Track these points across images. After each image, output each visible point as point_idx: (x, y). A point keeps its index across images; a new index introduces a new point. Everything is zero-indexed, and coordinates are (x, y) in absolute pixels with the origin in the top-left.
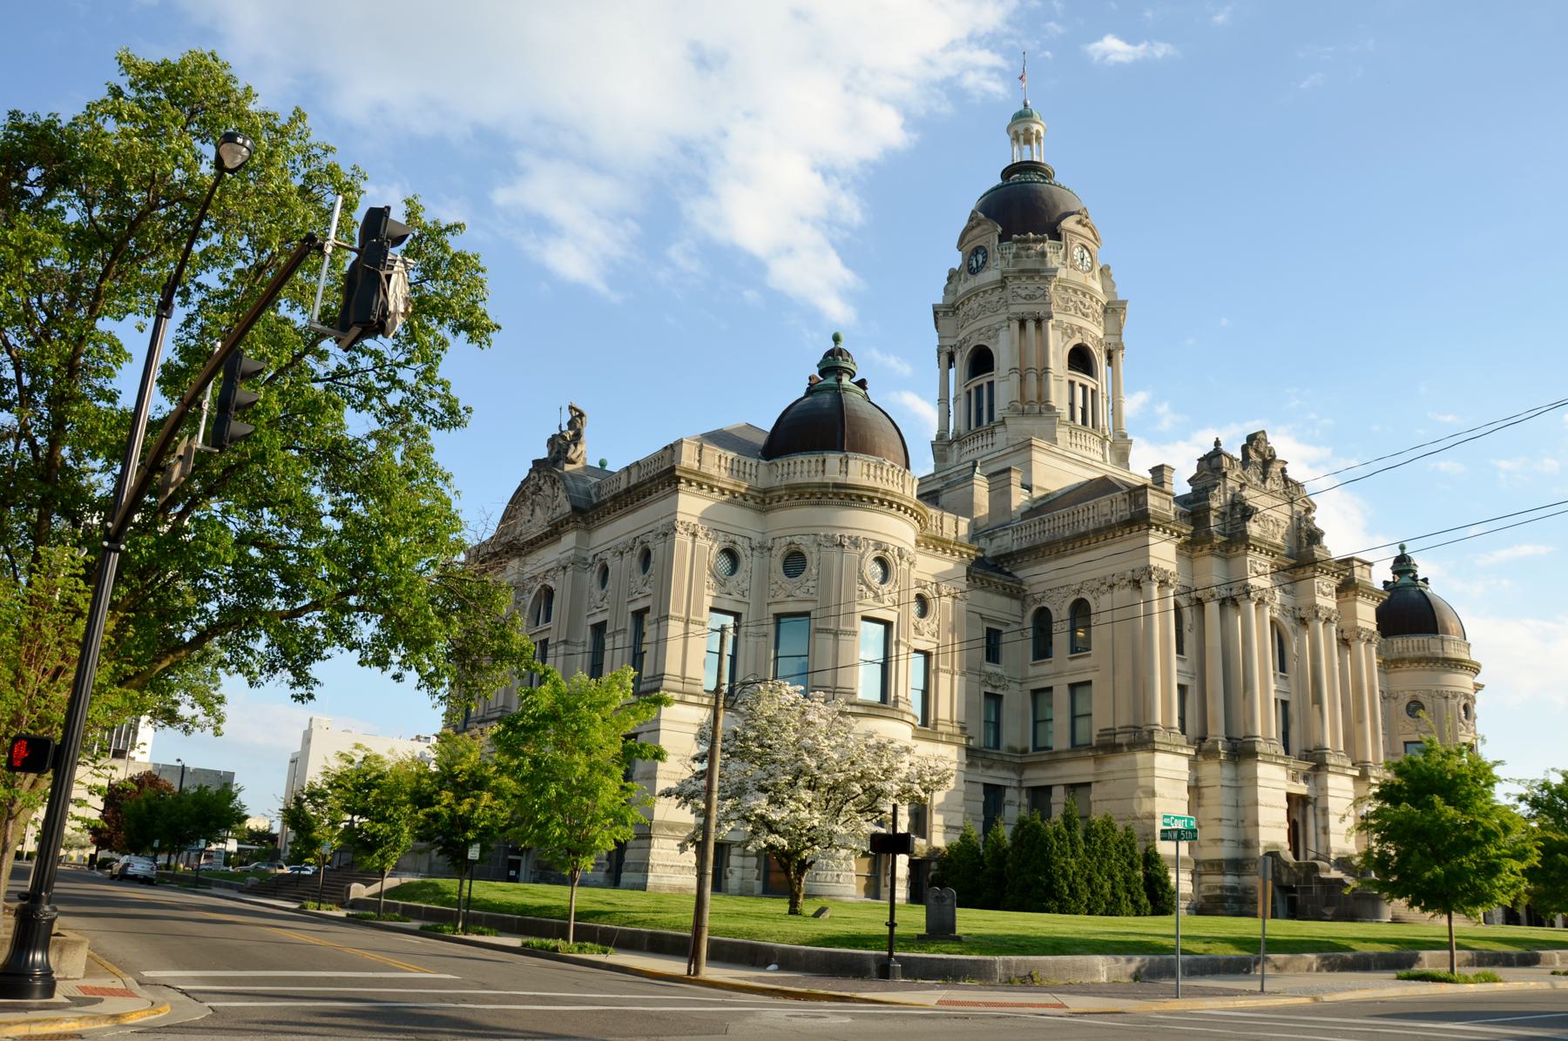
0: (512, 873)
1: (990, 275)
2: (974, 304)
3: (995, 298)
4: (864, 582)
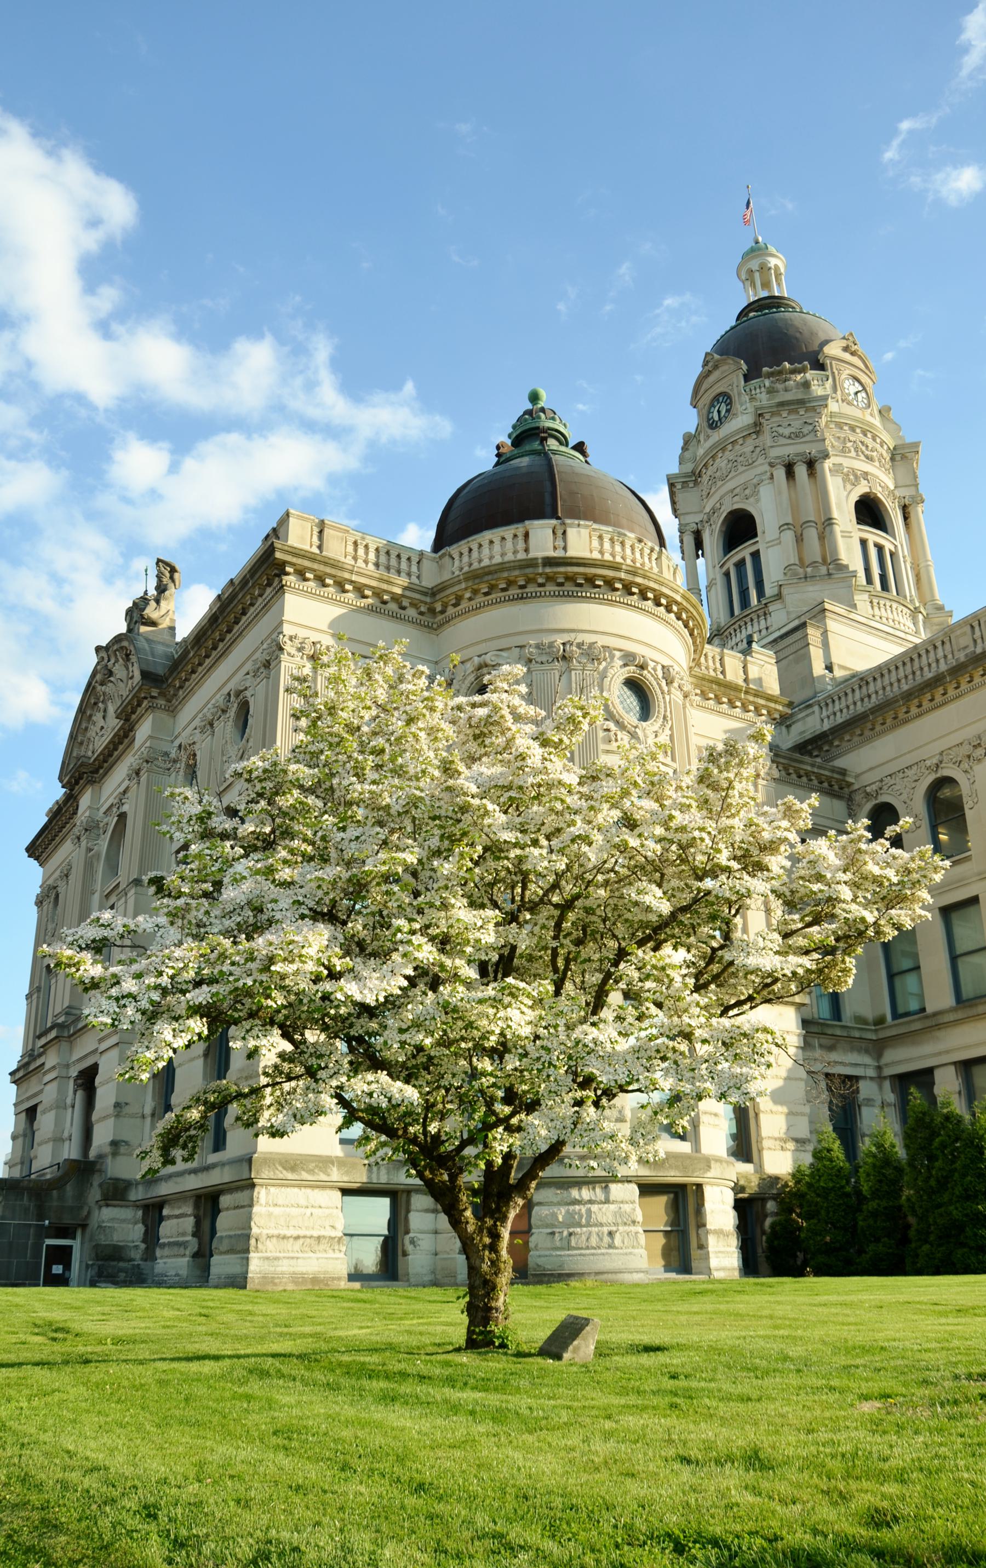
0: (57, 1269)
1: (742, 420)
2: (721, 462)
3: (748, 448)
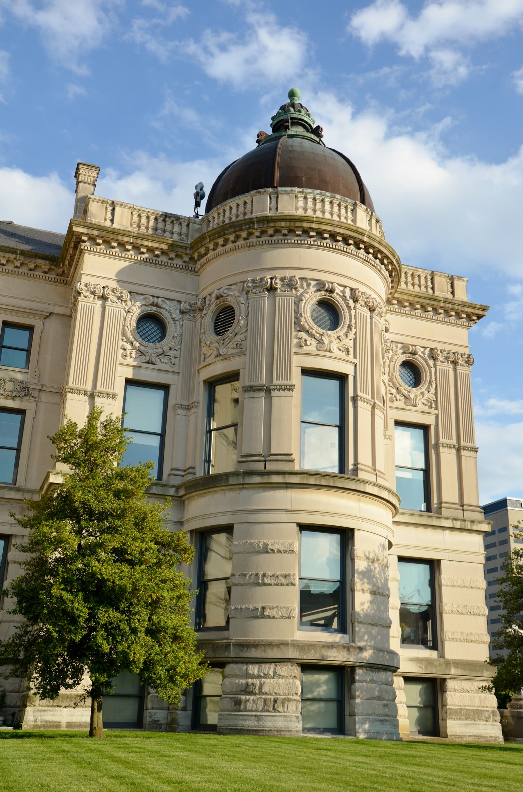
4: (302, 329)
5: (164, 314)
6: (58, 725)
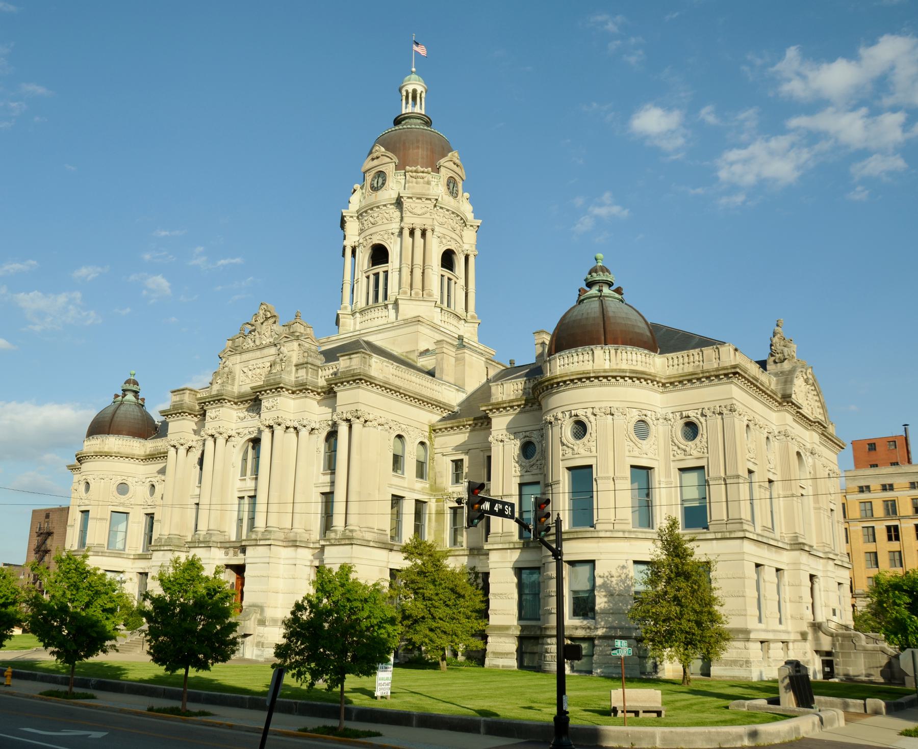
5: (648, 419)
6: (498, 666)
